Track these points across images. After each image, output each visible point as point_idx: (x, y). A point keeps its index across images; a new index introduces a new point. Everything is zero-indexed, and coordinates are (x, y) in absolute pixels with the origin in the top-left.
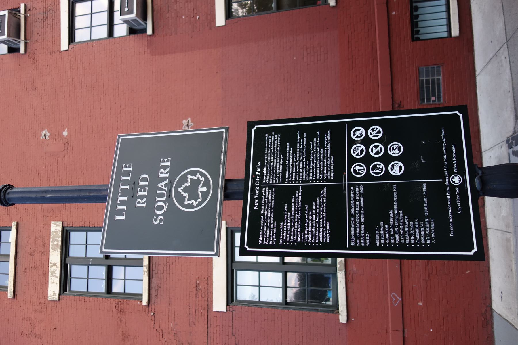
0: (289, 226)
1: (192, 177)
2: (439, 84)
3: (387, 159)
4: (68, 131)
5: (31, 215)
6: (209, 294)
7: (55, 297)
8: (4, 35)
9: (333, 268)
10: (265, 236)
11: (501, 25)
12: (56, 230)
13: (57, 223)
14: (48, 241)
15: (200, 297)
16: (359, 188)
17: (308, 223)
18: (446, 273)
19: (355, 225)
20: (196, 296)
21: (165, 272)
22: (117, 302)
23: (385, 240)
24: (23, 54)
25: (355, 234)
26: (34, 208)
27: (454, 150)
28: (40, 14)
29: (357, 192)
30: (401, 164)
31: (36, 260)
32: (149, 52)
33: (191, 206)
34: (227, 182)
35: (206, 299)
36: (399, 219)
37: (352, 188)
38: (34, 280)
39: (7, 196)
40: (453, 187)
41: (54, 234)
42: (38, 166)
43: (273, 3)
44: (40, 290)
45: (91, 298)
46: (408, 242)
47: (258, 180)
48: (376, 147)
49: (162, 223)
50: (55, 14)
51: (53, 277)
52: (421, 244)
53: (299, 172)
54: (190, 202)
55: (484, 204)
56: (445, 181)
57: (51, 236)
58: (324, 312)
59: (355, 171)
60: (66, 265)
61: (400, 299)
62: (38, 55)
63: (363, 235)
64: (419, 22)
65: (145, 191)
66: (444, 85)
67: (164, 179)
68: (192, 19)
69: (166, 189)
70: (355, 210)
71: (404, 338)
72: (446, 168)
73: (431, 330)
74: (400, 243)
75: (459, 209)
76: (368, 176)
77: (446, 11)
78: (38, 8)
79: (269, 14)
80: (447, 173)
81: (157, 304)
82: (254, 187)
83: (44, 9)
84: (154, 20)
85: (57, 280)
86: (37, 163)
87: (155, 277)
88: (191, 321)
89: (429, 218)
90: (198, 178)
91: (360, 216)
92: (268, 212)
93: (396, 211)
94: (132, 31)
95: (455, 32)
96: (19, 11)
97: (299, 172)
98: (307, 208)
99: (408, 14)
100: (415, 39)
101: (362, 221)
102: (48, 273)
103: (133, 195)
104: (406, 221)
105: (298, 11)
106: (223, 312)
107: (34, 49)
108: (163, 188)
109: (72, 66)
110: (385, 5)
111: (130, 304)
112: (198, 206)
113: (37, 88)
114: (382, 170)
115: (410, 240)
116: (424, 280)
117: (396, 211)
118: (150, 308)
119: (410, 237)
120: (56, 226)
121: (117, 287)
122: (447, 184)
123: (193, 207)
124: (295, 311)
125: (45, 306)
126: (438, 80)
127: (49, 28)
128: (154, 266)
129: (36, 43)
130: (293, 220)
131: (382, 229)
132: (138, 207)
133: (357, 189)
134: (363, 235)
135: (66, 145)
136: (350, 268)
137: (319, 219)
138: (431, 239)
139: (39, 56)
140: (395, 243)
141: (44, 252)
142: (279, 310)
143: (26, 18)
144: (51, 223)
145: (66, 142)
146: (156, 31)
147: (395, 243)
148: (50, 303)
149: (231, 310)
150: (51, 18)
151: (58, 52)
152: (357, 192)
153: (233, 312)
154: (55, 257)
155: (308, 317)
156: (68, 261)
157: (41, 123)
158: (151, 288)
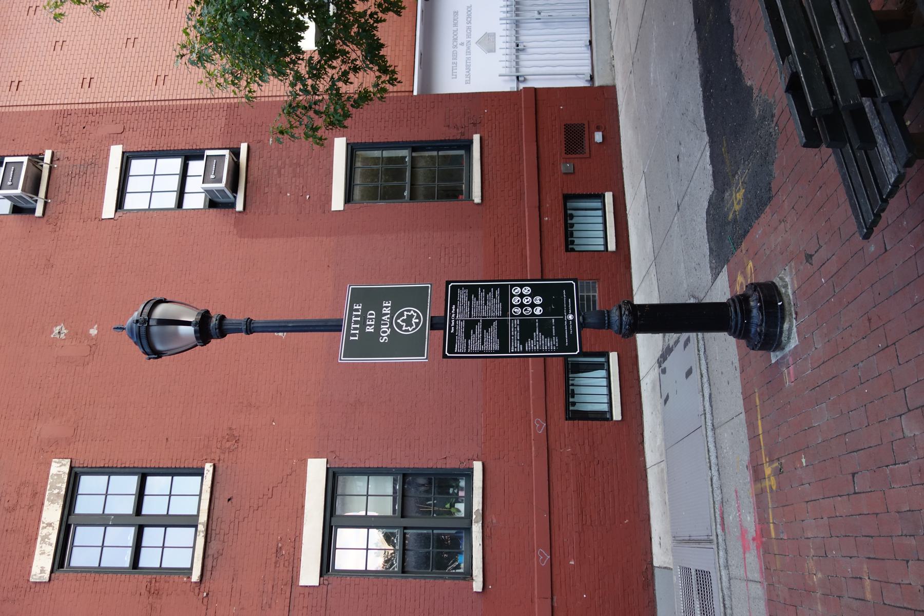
0: (474, 342)
1: (407, 313)
2: (594, 302)
3: (533, 305)
4: (98, 329)
5: (17, 450)
6: (295, 561)
7: (43, 576)
8: (17, 188)
9: (467, 521)
10: (459, 347)
11: (650, 243)
12: (59, 472)
13: (63, 462)
14: (43, 489)
15: (282, 566)
16: (517, 321)
17: (486, 340)
18: (602, 523)
19: (514, 341)
20: (275, 566)
21: (231, 532)
22: (148, 580)
23: (531, 348)
24: (39, 217)
25: (514, 345)
26: (24, 439)
27: (570, 302)
28: (75, 167)
29: (515, 323)
30: (541, 308)
31: (16, 518)
32: (235, 232)
33: (408, 331)
34: (432, 318)
35: (291, 569)
36: (539, 337)
37: (513, 321)
38: (8, 551)
39: (252, 325)
40: (568, 321)
41: (56, 477)
42: (41, 376)
43: (406, 192)
44: (17, 566)
45: (106, 576)
46: (543, 349)
47: (453, 316)
48: (527, 299)
49: (387, 341)
50: (100, 169)
51: (44, 545)
52: (550, 349)
53: (480, 312)
54: (407, 328)
55: (643, 441)
56: (564, 317)
57: (50, 480)
58: (453, 579)
59: (514, 312)
60: (68, 527)
61: (549, 557)
62: (63, 220)
63: (518, 346)
64: (574, 232)
65: (372, 321)
66: (600, 303)
67: (387, 314)
68: (300, 198)
69: (389, 320)
70: (514, 333)
71: (552, 607)
72: (565, 311)
73: (585, 596)
74: (539, 349)
75: (571, 332)
76: (522, 315)
77: (602, 223)
78: (72, 159)
79: (400, 204)
80: (565, 314)
81: (214, 580)
82: (450, 320)
83: (83, 162)
84: (247, 194)
85: (51, 550)
86: (39, 372)
87: (215, 540)
88: (265, 602)
89: (555, 336)
90: (412, 314)
91: (517, 336)
92: (461, 334)
93: (537, 333)
94: (212, 204)
95: (612, 246)
96: (42, 159)
97: (480, 312)
98: (485, 332)
99: (562, 222)
100: (569, 250)
101: (518, 338)
102: (36, 539)
103: (363, 324)
104: (543, 338)
105: (436, 203)
106: (314, 586)
107: (57, 212)
108: (386, 319)
109: (116, 240)
110: (537, 209)
111: (171, 582)
112: (412, 331)
113: (54, 266)
114: (530, 311)
115: (545, 348)
116: (577, 532)
117: (537, 333)
118: (203, 586)
119: (545, 346)
120: (60, 466)
121: (148, 559)
122: (566, 319)
123: (409, 331)
124: (415, 580)
125: (23, 592)
126: (594, 296)
127: (87, 187)
128: (214, 523)
129: (62, 205)
130: (476, 339)
131: (529, 342)
132: (368, 332)
133: (515, 322)
134: (518, 346)
135: (93, 348)
136: (488, 520)
137: (493, 338)
138: (556, 347)
139: (64, 222)
140: (536, 349)
141: (33, 505)
142: (394, 579)
143: (51, 169)
144: (52, 461)
145: (94, 345)
146: (248, 207)
147: (536, 349)
148: (33, 586)
149: (326, 582)
150: (92, 175)
151: (97, 220)
152: (515, 323)
153: (329, 585)
154: (52, 513)
155: (432, 586)
156: (72, 520)
157: (54, 315)
158: (206, 556)
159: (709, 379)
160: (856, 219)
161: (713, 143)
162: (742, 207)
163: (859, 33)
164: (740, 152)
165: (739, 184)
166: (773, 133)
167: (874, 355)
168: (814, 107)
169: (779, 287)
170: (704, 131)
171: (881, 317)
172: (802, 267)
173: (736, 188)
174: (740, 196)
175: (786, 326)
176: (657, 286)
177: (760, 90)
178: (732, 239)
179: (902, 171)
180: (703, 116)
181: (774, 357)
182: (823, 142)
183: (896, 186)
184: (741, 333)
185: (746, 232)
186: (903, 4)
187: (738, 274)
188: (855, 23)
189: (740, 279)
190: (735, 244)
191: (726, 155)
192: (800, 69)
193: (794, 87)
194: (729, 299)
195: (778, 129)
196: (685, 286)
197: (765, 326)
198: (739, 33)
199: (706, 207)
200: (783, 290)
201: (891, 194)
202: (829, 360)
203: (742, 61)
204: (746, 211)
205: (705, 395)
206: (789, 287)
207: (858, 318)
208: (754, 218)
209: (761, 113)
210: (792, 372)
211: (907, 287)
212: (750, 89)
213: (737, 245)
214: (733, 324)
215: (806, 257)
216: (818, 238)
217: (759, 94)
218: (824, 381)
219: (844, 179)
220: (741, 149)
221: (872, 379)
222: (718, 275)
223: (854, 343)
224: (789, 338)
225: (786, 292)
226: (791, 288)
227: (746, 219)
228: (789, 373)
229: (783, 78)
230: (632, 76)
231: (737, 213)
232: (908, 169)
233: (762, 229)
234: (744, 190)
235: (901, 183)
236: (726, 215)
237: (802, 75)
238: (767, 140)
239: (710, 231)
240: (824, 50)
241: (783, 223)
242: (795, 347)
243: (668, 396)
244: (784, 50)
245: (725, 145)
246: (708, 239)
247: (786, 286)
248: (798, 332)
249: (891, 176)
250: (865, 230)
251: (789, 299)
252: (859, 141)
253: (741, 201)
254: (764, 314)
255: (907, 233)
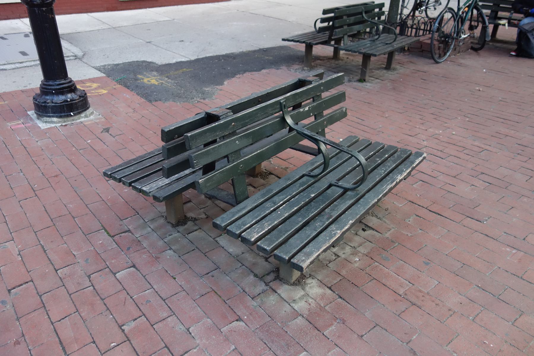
11: (125, 24)
159: (18, 68)
160: (119, 165)
161: (190, 63)
162: (145, 84)
163: (246, 158)
164: (182, 80)
165: (161, 81)
166: (193, 100)
167: (29, 183)
168: (191, 136)
169: (85, 112)
170: (198, 56)
171: (58, 184)
172: (100, 126)
173: (159, 79)
174: (154, 82)
175: (55, 119)
176: (94, 29)
177: (221, 90)
178: (124, 78)
179: (150, 194)
180: (208, 55)
181: (32, 113)
182: (166, 143)
183: (140, 191)
184: (45, 90)
185: (128, 87)
186: (265, 171)
187: (99, 84)
188: (253, 154)
189: (95, 85)
190: (120, 81)
191: (181, 71)
192: (222, 122)
193: (210, 118)
194: (71, 79)
195: (195, 103)
196: (93, 49)
197: (52, 106)
198: (256, 75)
199: (148, 60)
200: (83, 115)
201: (135, 188)
202: (27, 151)
203: (239, 78)
204: (143, 86)
205: (5, 66)
206: (86, 119)
207: (58, 168)
208: (137, 92)
209: (207, 91)
210: (19, 126)
211: (79, 199)
212: (222, 84)
213: (120, 82)
214: (51, 83)
215: (108, 128)
216: (120, 135)
217: (219, 89)
218: (10, 150)
219: (150, 153)
220: (184, 81)
221: (9, 184)
222: (99, 71)
223: (39, 168)
224: (46, 122)
225: (82, 117)
226: (85, 120)
227: (137, 86)
228: (18, 124)
229: (216, 109)
230: (236, 11)
231: (142, 81)
232: (152, 198)
233: (129, 97)
234: (157, 84)
235: (142, 194)
236: (140, 73)
237: (217, 124)
238: (189, 96)
239: (131, 64)
240: (235, 137)
241: (133, 111)
242: (39, 127)
243: (5, 39)
244: (235, 109)
245: (187, 70)
246: (126, 63)
247: (86, 116)
248: (51, 128)
249: (148, 187)
250: (109, 173)
251: (77, 120)
252: (168, 167)
253: (149, 83)
254: (62, 104)
255: (119, 193)
